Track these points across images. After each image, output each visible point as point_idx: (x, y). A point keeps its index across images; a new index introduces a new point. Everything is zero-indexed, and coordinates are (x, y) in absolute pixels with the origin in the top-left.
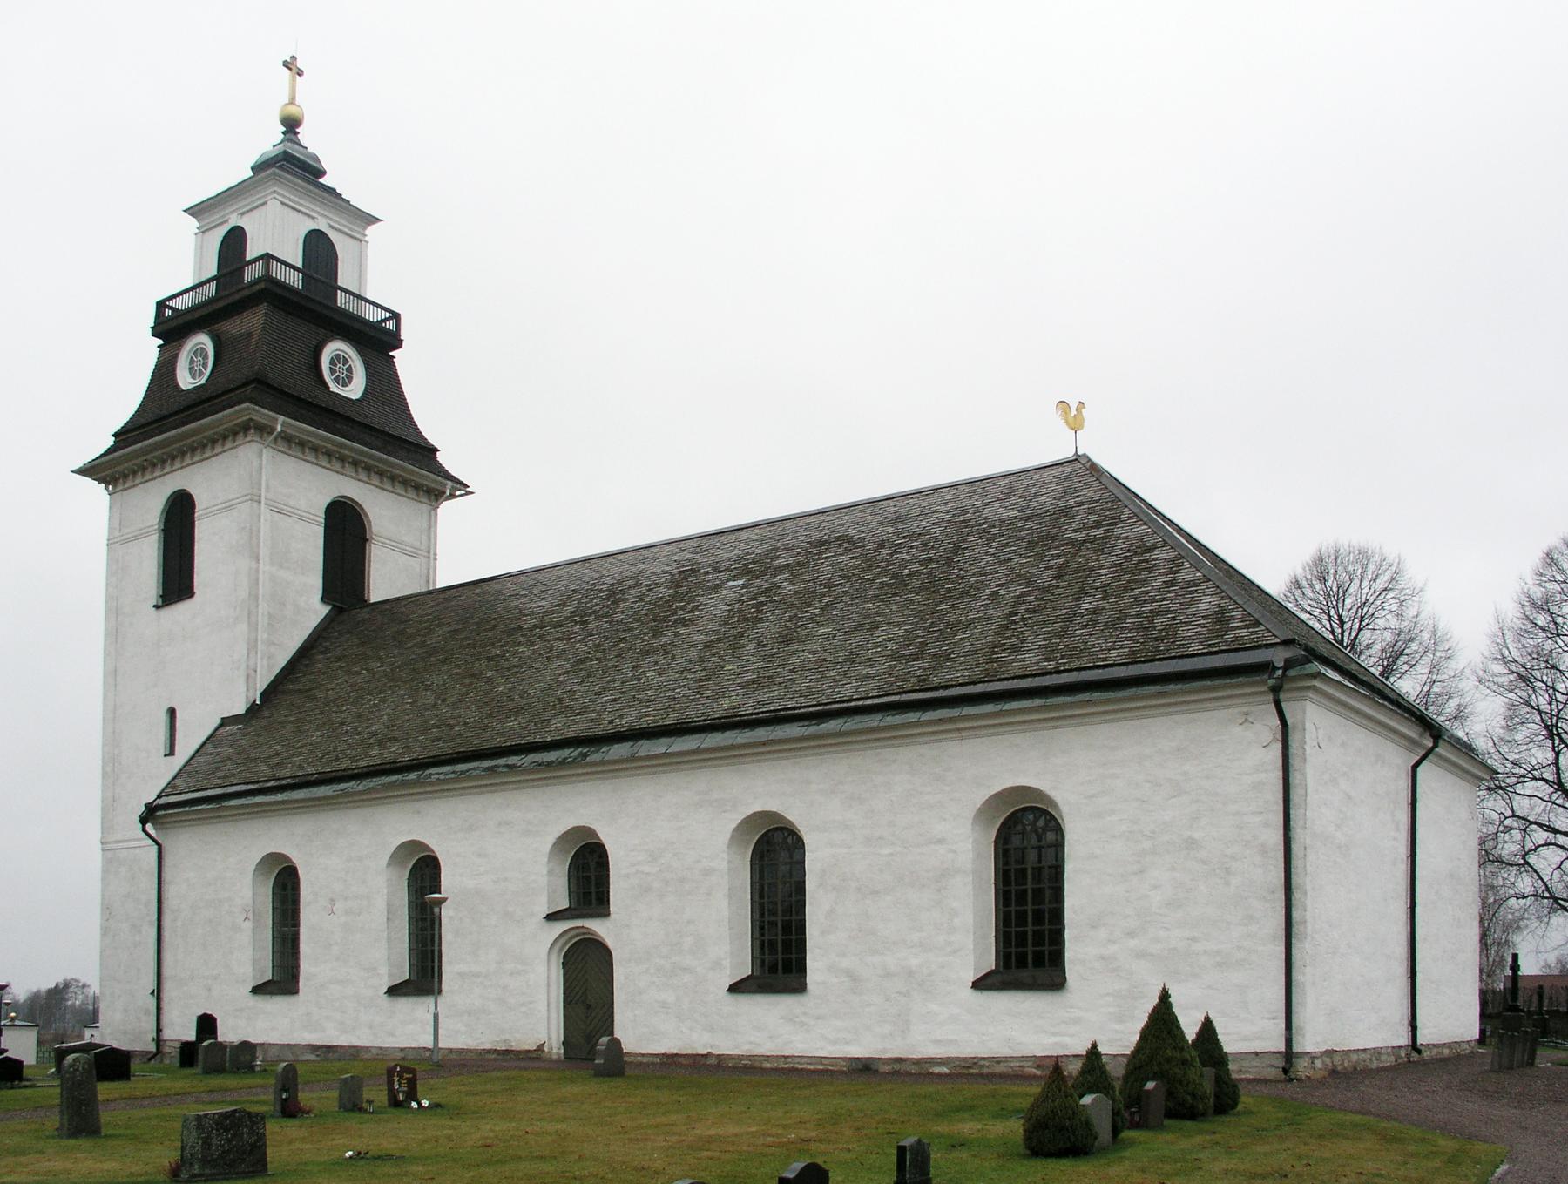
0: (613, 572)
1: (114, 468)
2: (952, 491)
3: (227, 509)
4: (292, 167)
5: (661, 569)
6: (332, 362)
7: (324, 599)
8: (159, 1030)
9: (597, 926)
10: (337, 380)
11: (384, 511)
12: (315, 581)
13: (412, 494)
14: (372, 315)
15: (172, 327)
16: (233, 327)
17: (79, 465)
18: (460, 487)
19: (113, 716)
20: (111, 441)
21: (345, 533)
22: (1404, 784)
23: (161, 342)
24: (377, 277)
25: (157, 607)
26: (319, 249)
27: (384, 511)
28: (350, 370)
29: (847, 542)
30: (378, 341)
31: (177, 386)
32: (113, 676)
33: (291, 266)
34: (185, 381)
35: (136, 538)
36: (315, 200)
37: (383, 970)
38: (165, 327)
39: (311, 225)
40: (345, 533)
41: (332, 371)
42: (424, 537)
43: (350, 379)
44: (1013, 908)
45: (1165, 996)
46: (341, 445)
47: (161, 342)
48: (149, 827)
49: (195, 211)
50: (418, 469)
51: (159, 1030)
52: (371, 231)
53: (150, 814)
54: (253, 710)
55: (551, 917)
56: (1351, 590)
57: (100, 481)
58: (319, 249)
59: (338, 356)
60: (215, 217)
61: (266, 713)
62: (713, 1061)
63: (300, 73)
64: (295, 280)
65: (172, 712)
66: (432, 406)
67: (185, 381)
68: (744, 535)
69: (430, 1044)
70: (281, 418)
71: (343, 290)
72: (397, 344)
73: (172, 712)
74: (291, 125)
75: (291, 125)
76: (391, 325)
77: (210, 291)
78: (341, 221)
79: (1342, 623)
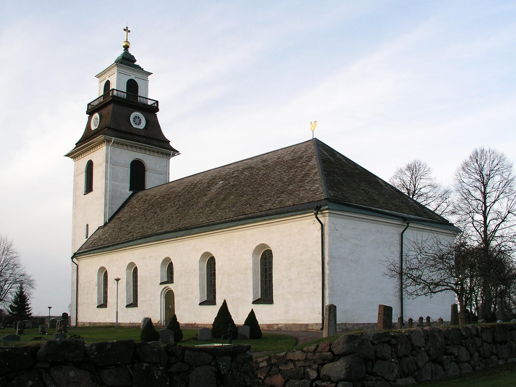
0: (197, 179)
1: (73, 155)
2: (281, 151)
3: (100, 165)
4: (127, 60)
5: (209, 177)
6: (134, 118)
7: (130, 190)
8: (77, 319)
9: (170, 286)
10: (136, 124)
11: (150, 161)
12: (128, 185)
13: (161, 155)
14: (150, 103)
15: (91, 111)
16: (104, 111)
17: (66, 153)
18: (175, 152)
19: (74, 227)
20: (75, 146)
21: (138, 171)
22: (398, 238)
23: (89, 116)
24: (153, 91)
25: (84, 194)
26: (132, 86)
27: (150, 161)
28: (140, 120)
29: (251, 168)
30: (151, 110)
31: (91, 129)
32: (75, 215)
33: (122, 92)
34: (93, 128)
35: (80, 174)
36: (130, 70)
37: (125, 300)
38: (89, 112)
39: (129, 78)
40: (138, 171)
41: (134, 121)
42: (165, 169)
43: (140, 123)
44: (268, 279)
45: (225, 301)
46: (134, 144)
47: (89, 116)
48: (74, 260)
49: (98, 76)
50: (165, 149)
51: (77, 319)
52: (149, 77)
53: (75, 256)
54: (106, 224)
55: (161, 284)
56: (485, 167)
57: (72, 158)
58: (132, 86)
59: (136, 117)
60: (102, 78)
61: (109, 225)
62: (196, 326)
63: (129, 31)
64: (124, 96)
65: (87, 225)
66: (167, 132)
67: (93, 128)
68: (230, 166)
69: (115, 322)
70: (113, 138)
71: (140, 97)
72: (157, 110)
73: (87, 225)
74: (126, 47)
75: (126, 47)
76: (155, 105)
77: (102, 99)
78: (139, 75)
79: (483, 178)
